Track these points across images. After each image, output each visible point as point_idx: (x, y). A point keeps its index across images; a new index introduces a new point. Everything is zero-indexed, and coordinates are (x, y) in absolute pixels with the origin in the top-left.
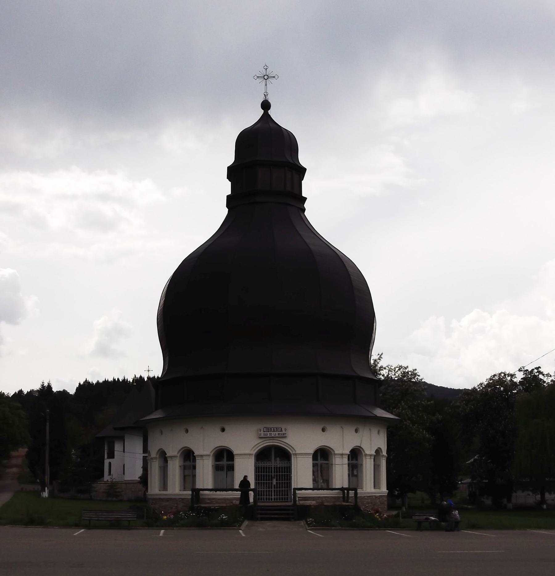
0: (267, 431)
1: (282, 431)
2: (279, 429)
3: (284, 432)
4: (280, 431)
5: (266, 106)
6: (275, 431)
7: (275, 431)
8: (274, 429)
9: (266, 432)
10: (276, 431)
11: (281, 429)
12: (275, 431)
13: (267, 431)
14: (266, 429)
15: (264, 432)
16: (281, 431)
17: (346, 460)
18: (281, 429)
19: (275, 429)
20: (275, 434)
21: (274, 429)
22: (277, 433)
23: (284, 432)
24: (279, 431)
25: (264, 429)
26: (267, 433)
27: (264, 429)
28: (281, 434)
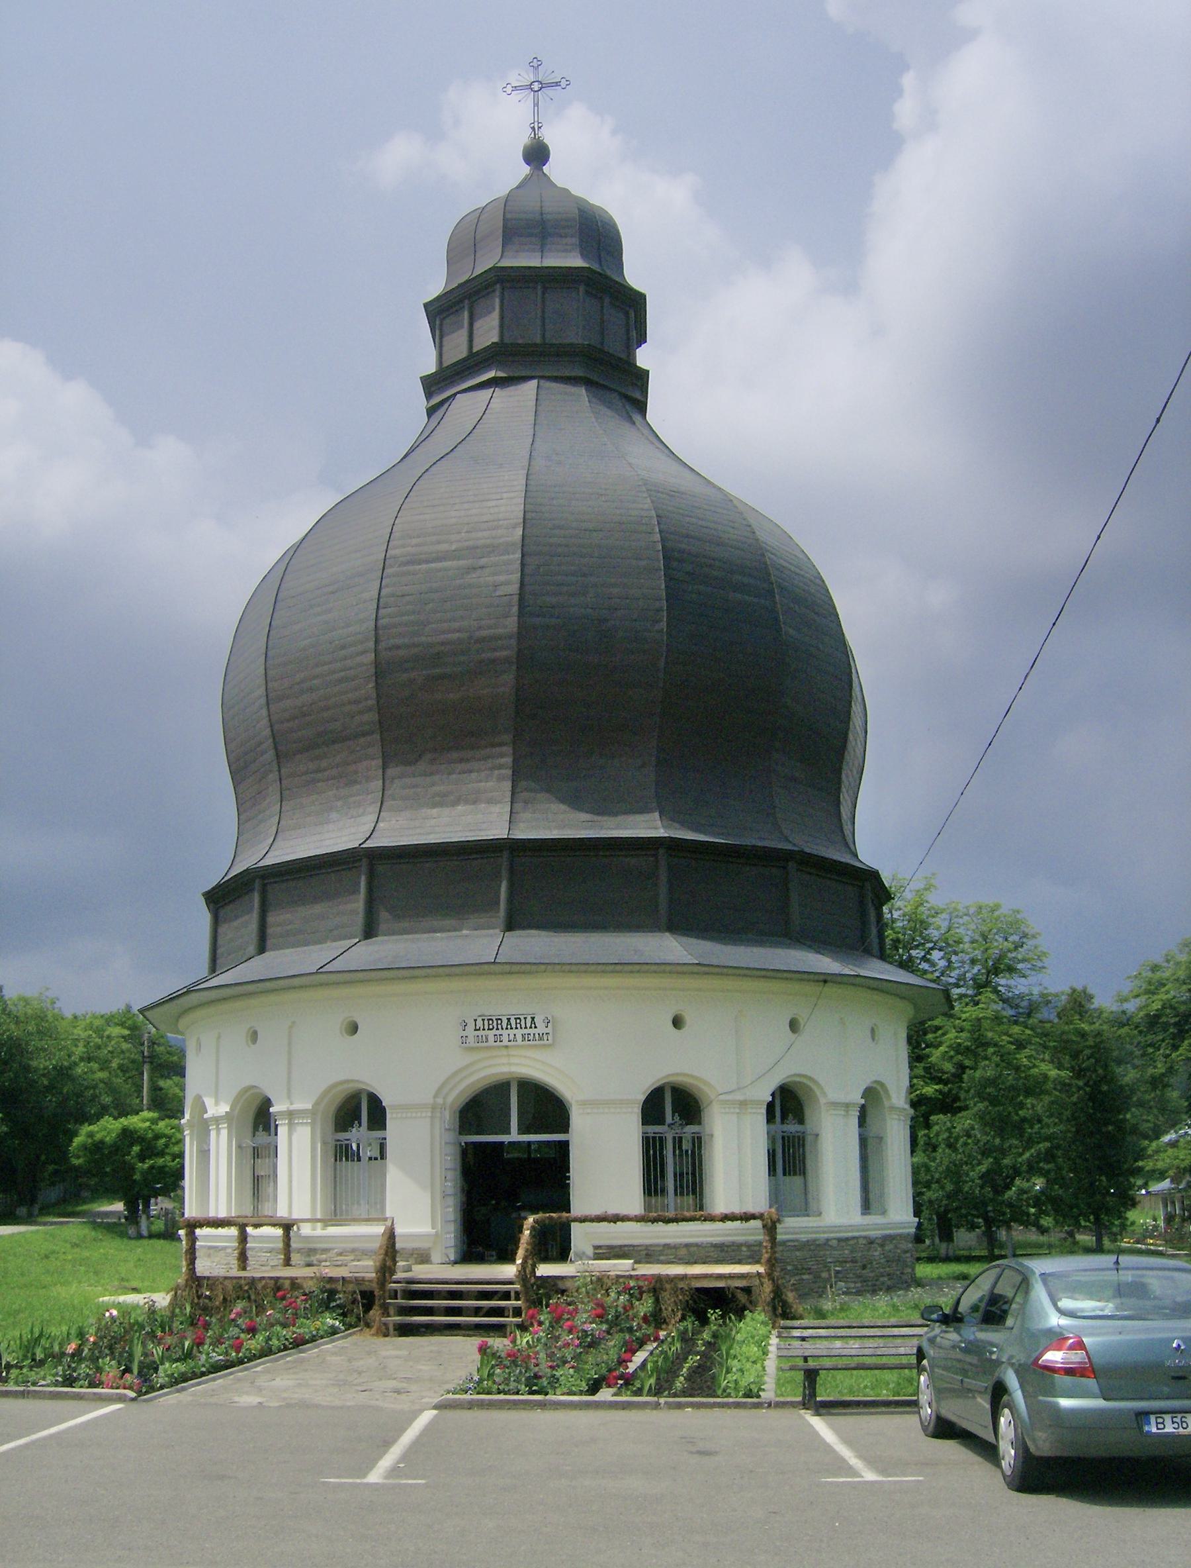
0: (486, 1027)
1: (536, 1027)
2: (525, 1018)
3: (541, 1029)
4: (528, 1025)
5: (537, 154)
6: (512, 1028)
7: (514, 1026)
8: (509, 1020)
9: (484, 1029)
10: (516, 1028)
11: (533, 1019)
12: (514, 1026)
13: (486, 1027)
14: (483, 1020)
15: (476, 1030)
16: (531, 1027)
17: (758, 1124)
18: (533, 1019)
19: (513, 1022)
20: (512, 1037)
21: (509, 1020)
22: (519, 1032)
23: (541, 1029)
24: (526, 1028)
25: (475, 1020)
26: (487, 1032)
27: (475, 1020)
28: (531, 1037)
